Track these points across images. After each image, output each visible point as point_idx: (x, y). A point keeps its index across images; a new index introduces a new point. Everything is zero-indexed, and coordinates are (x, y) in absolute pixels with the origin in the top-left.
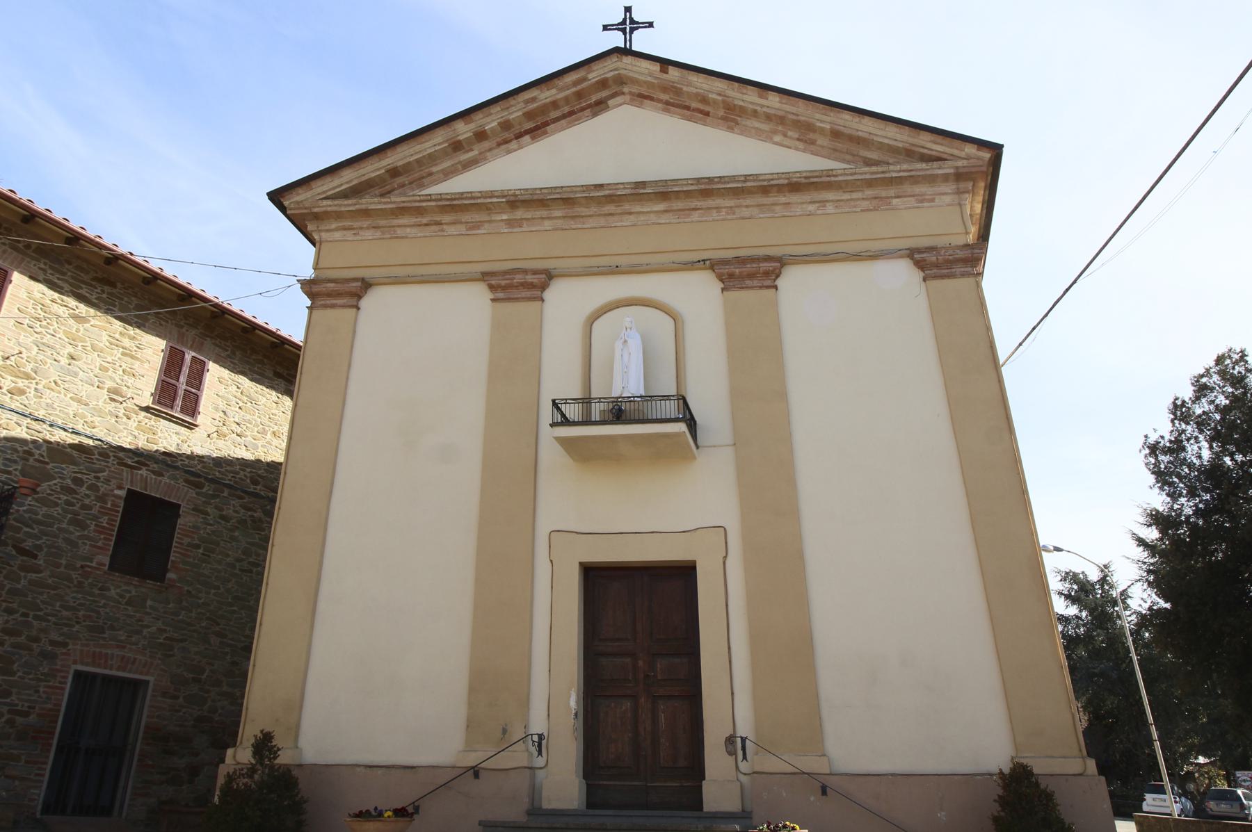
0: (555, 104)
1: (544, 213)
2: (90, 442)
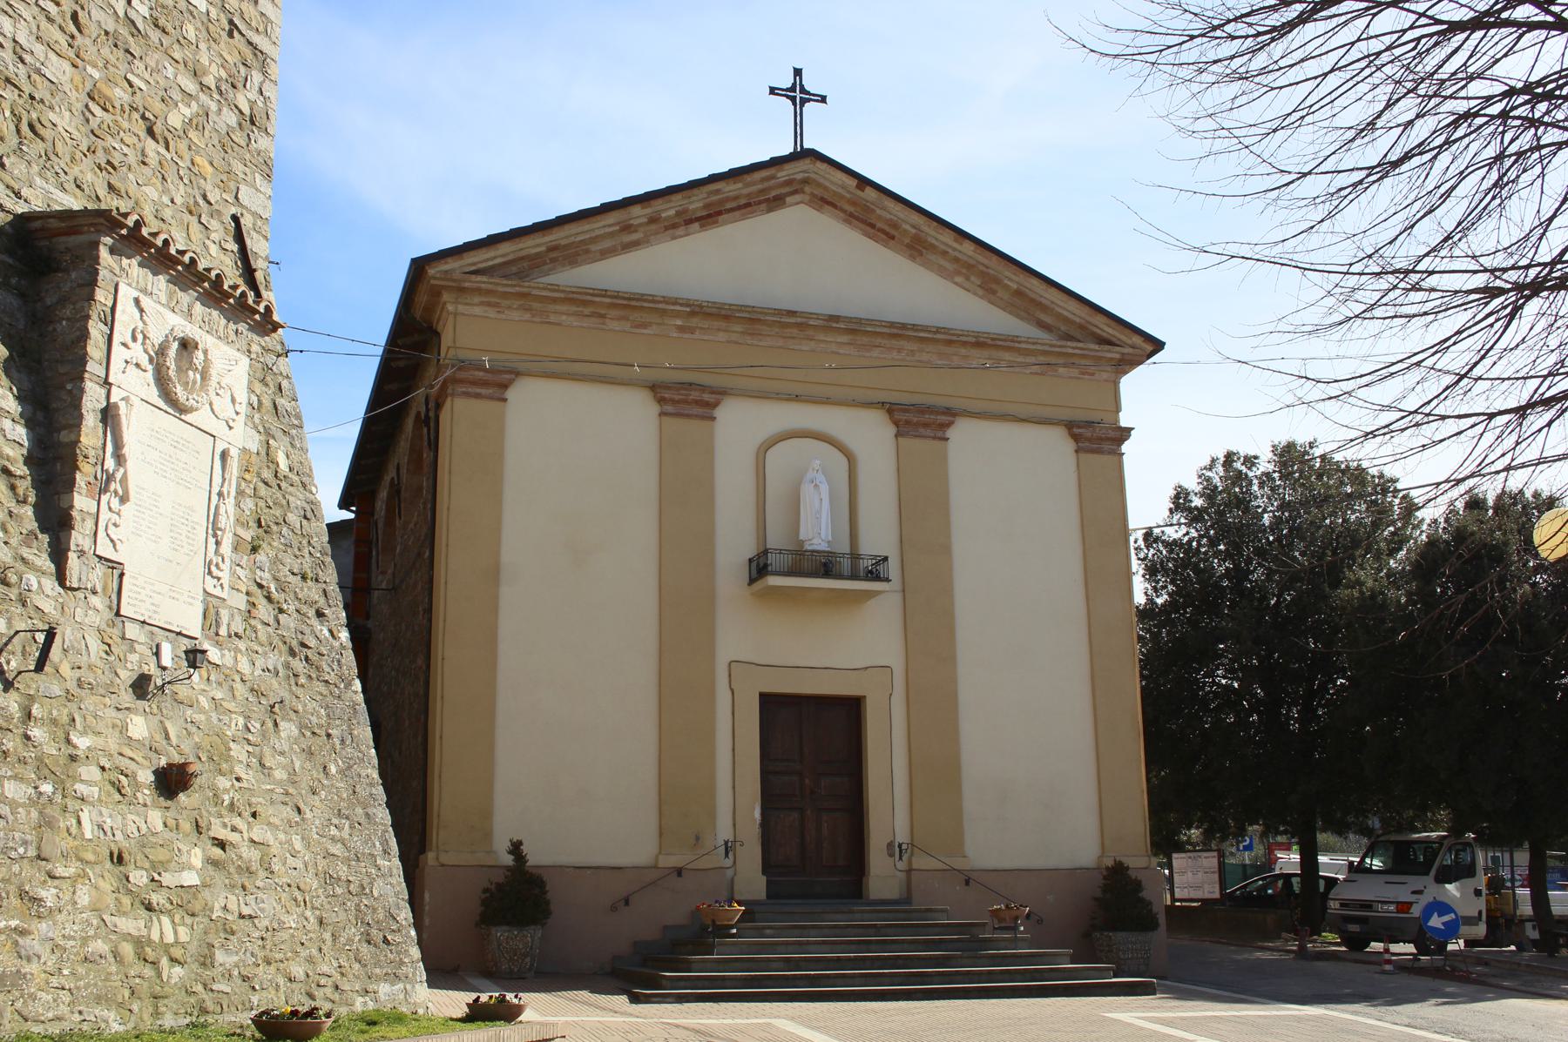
0: (736, 198)
1: (723, 324)
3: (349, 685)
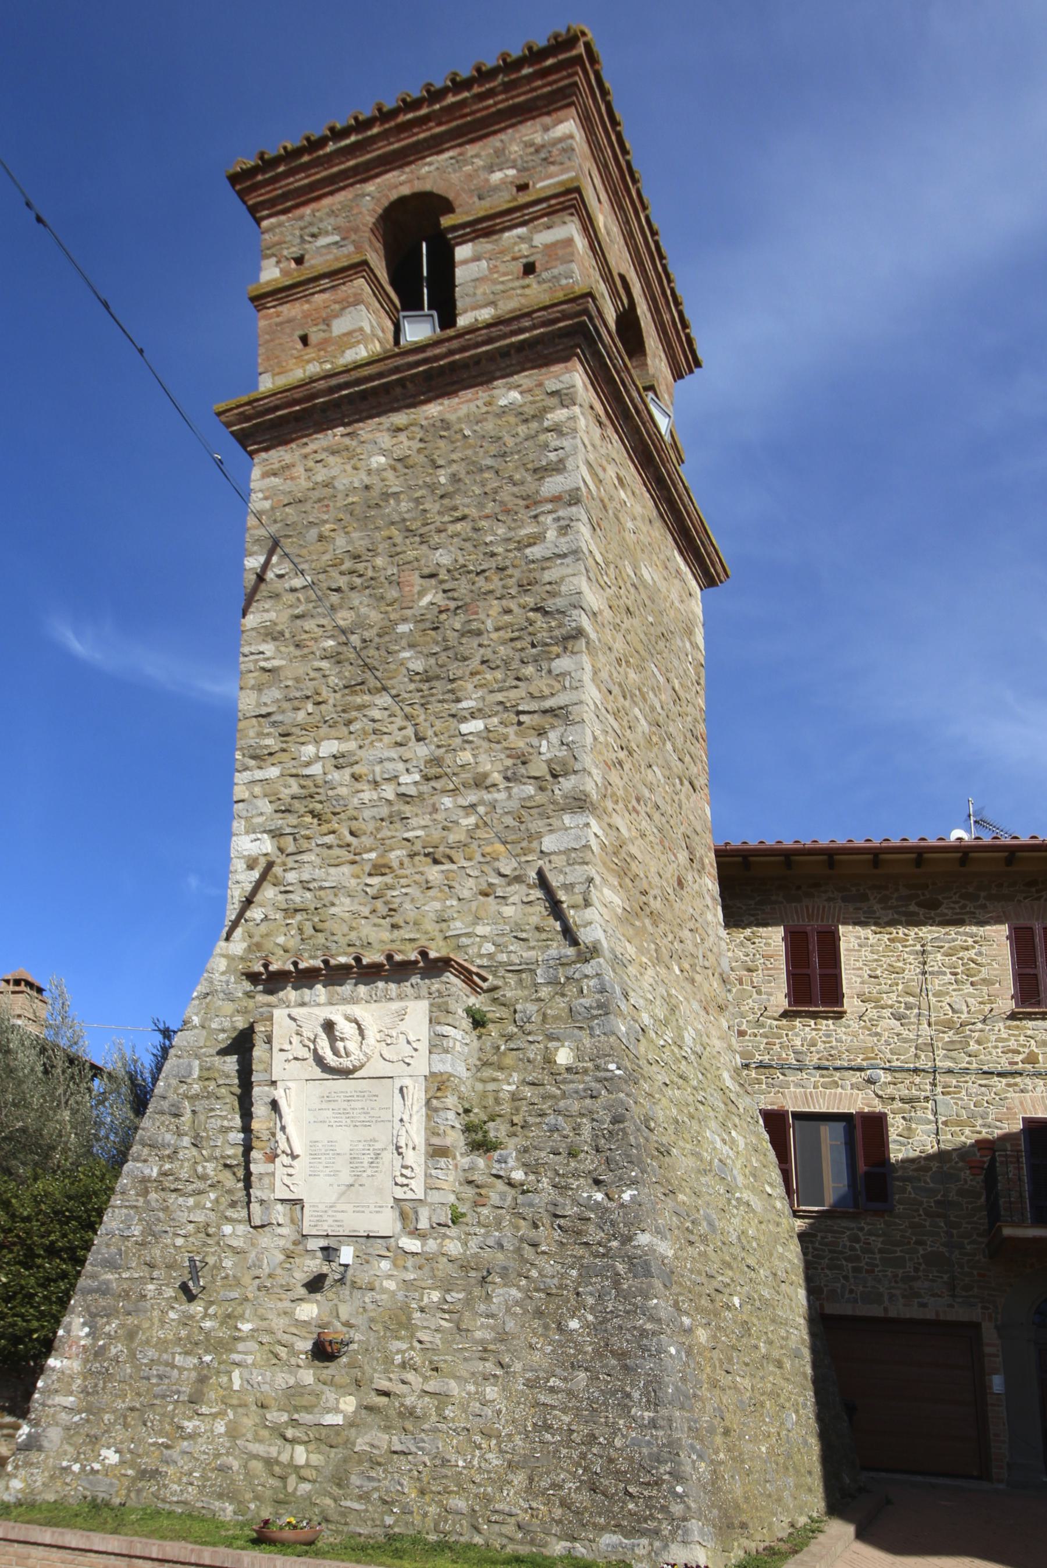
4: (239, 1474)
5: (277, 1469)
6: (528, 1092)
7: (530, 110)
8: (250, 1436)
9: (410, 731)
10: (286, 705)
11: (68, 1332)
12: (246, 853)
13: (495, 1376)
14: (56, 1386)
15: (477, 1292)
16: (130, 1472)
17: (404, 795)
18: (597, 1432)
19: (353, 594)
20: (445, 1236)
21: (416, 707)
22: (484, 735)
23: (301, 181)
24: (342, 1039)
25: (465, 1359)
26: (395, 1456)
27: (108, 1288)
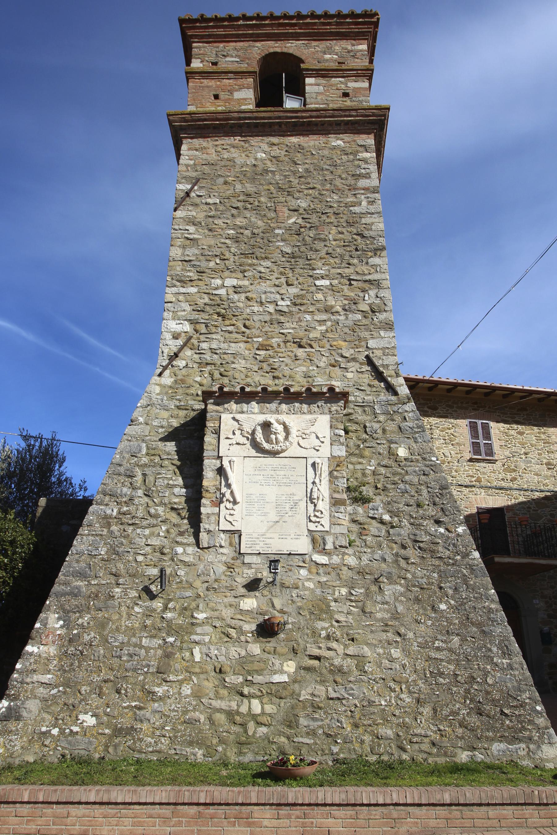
2: (549, 494)
3: (466, 555)
4: (204, 724)
5: (238, 718)
6: (383, 470)
7: (346, 36)
8: (212, 695)
9: (283, 280)
10: (202, 258)
11: (45, 625)
12: (173, 330)
13: (396, 642)
14: (34, 667)
15: (374, 588)
16: (107, 731)
17: (280, 311)
18: (475, 675)
19: (245, 212)
20: (344, 554)
21: (287, 269)
22: (330, 287)
23: (221, 32)
24: (275, 433)
25: (372, 632)
26: (331, 702)
27: (79, 591)
